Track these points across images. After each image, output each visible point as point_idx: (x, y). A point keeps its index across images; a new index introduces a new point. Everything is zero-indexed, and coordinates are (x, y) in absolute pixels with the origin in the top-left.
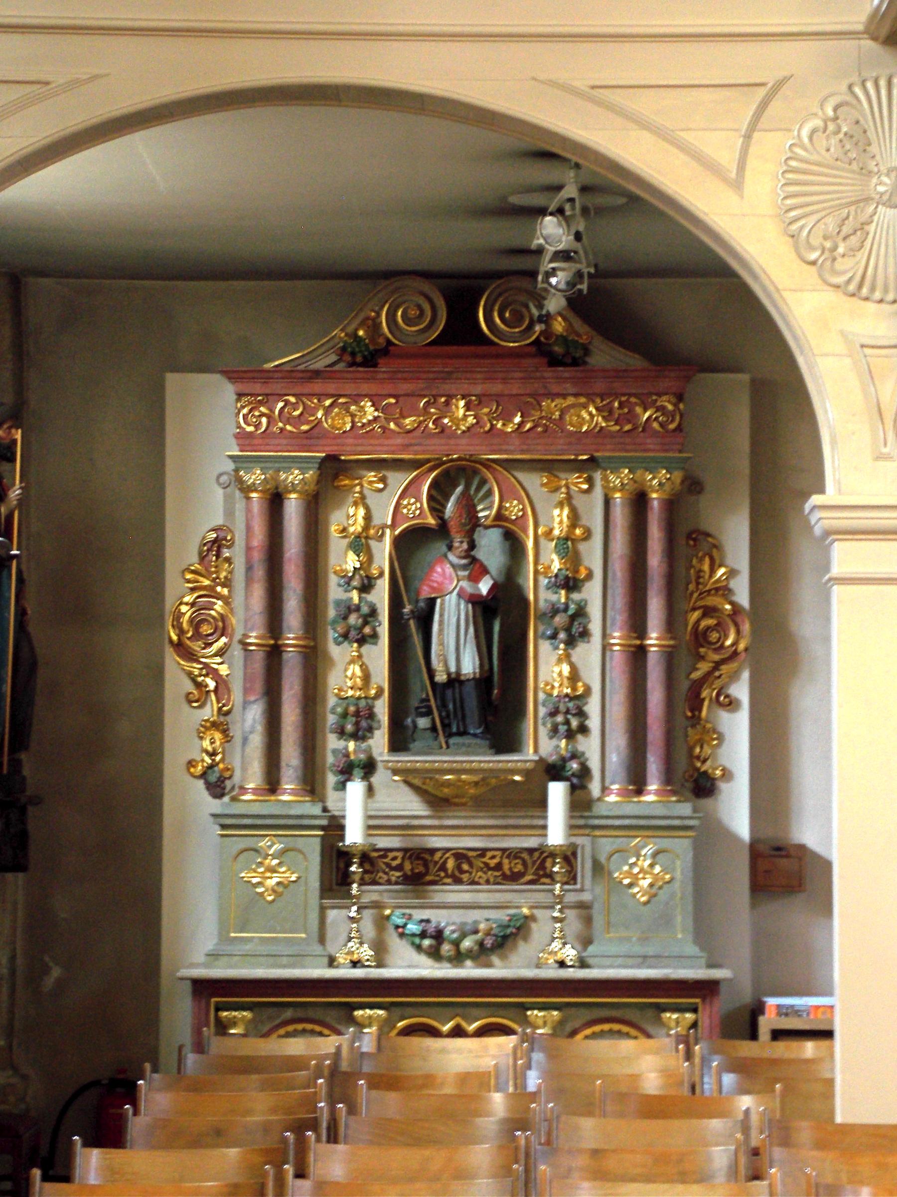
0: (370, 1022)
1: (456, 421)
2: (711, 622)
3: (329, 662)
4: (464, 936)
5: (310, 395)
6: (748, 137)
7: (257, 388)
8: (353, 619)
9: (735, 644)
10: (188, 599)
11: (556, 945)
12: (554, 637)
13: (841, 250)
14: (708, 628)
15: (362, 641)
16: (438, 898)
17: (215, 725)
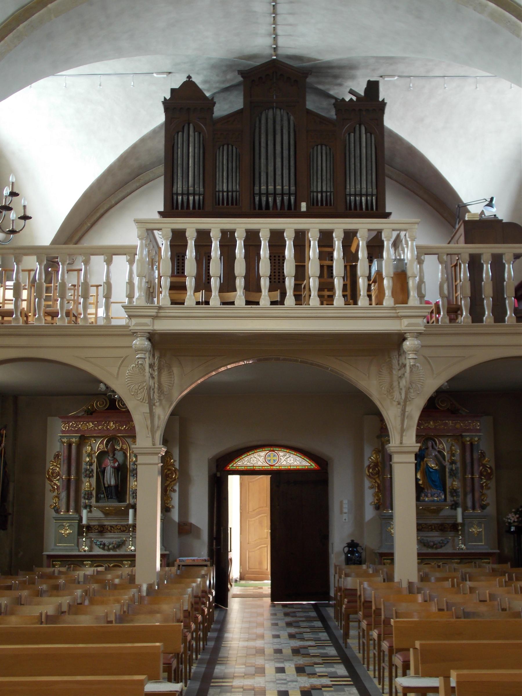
0: (87, 564)
1: (111, 427)
2: (169, 472)
3: (82, 482)
4: (110, 544)
5: (78, 422)
6: (119, 368)
7: (66, 420)
8: (88, 472)
9: (175, 477)
10: (51, 468)
11: (130, 547)
12: (133, 476)
13: (139, 392)
14: (169, 474)
15: (90, 477)
16: (107, 536)
17: (56, 497)
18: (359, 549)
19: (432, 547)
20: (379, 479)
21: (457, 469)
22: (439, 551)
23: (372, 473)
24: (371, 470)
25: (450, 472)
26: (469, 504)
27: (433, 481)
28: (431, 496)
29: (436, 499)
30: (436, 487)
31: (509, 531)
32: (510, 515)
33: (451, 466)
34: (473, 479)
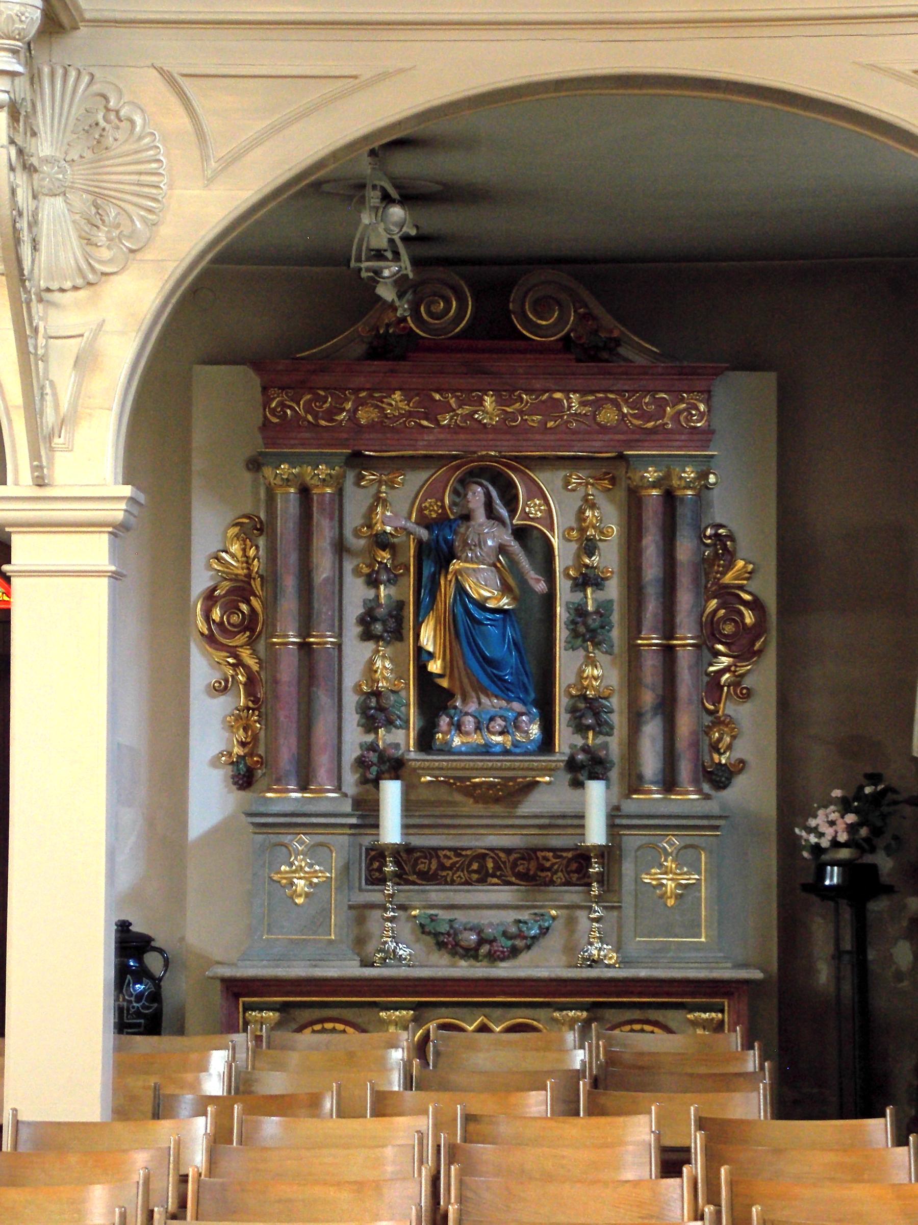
18: (153, 962)
19: (471, 953)
20: (254, 653)
21: (603, 610)
22: (504, 970)
23: (221, 624)
24: (216, 614)
25: (572, 625)
26: (650, 763)
27: (487, 662)
28: (478, 728)
29: (499, 739)
30: (504, 689)
31: (816, 887)
32: (821, 812)
33: (577, 597)
34: (668, 652)
